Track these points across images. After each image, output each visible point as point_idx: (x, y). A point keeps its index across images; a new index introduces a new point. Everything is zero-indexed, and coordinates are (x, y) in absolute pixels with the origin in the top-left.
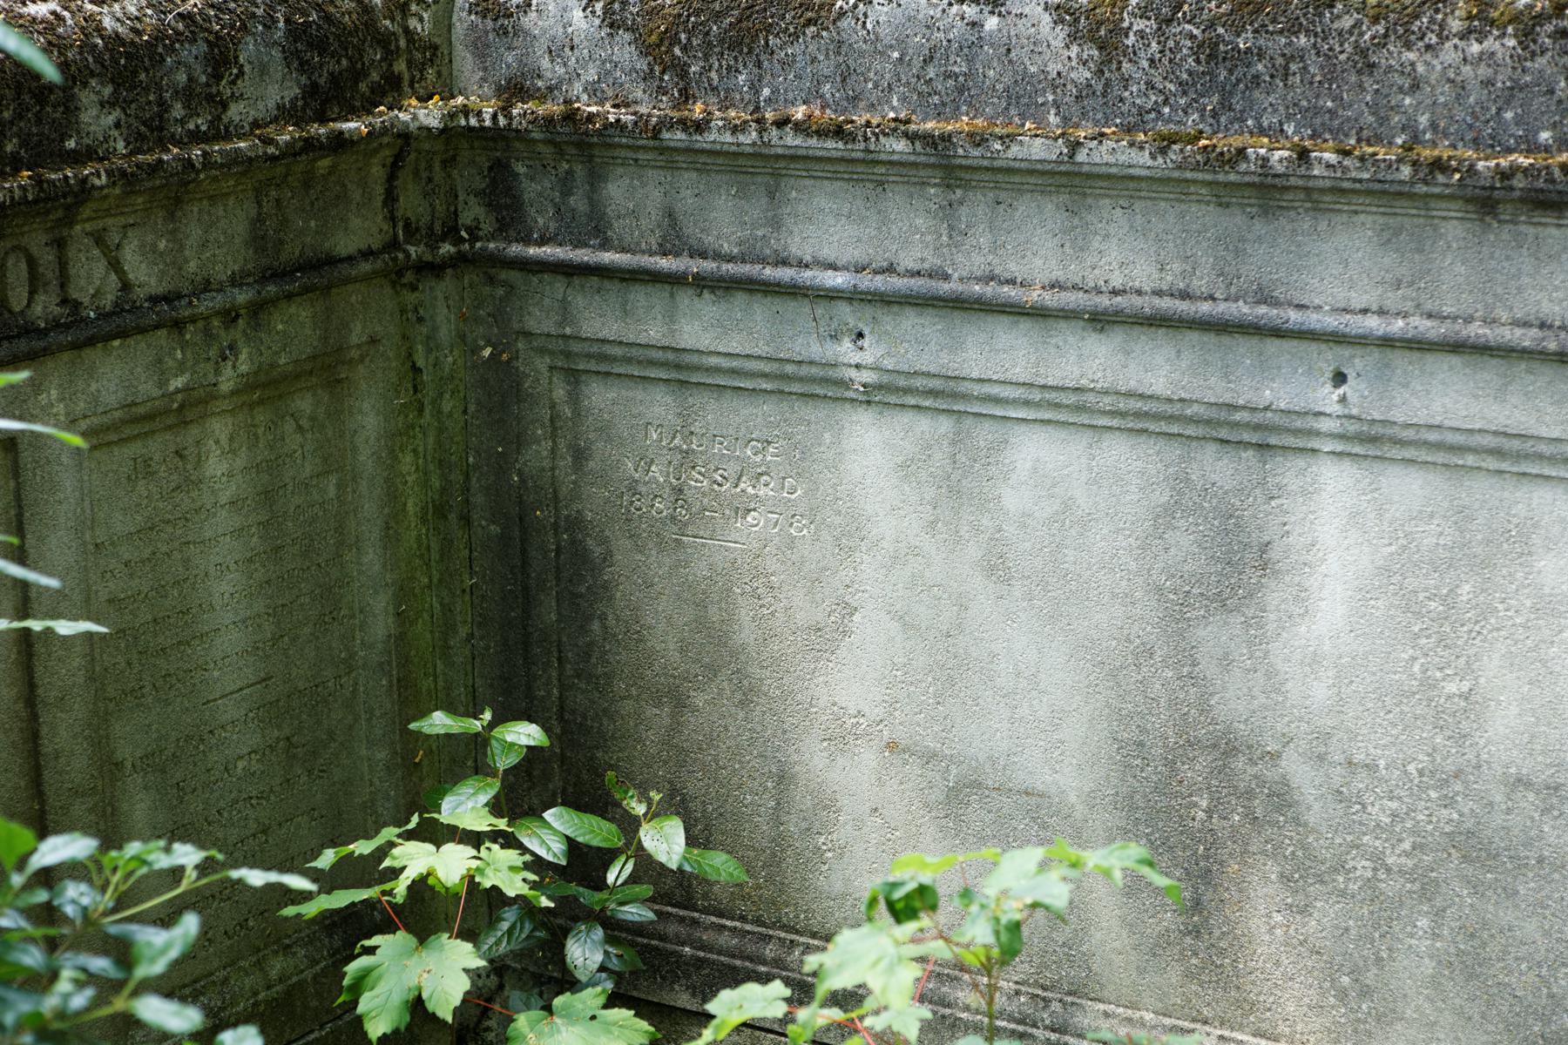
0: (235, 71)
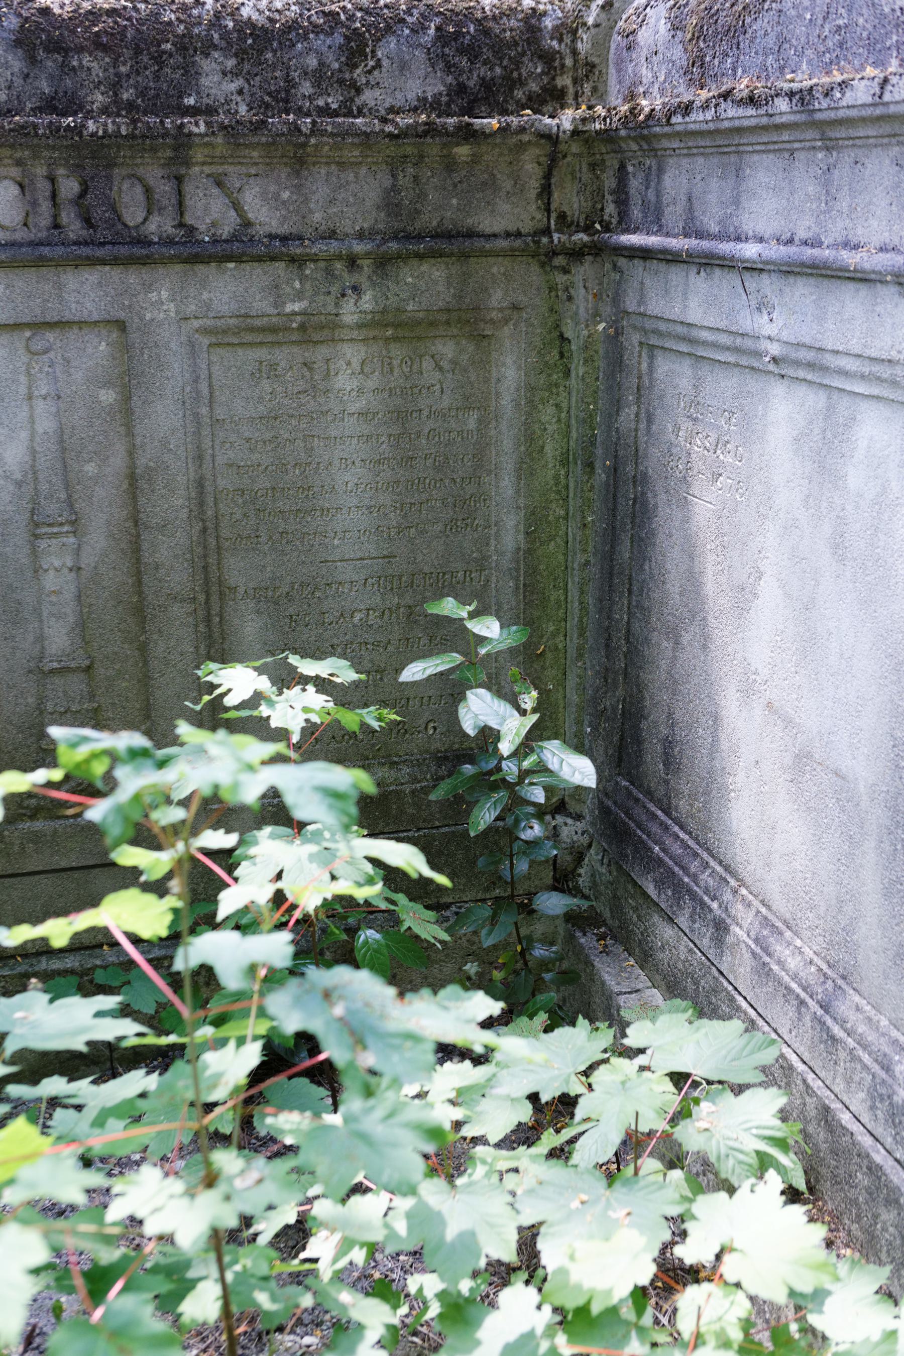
0: (371, 63)
